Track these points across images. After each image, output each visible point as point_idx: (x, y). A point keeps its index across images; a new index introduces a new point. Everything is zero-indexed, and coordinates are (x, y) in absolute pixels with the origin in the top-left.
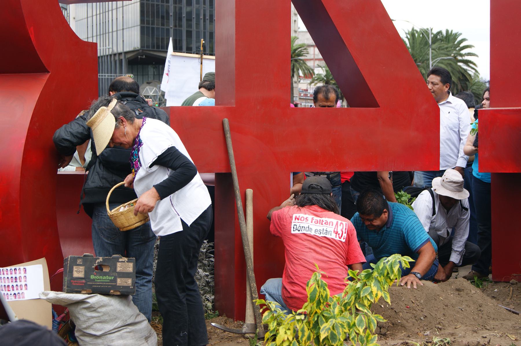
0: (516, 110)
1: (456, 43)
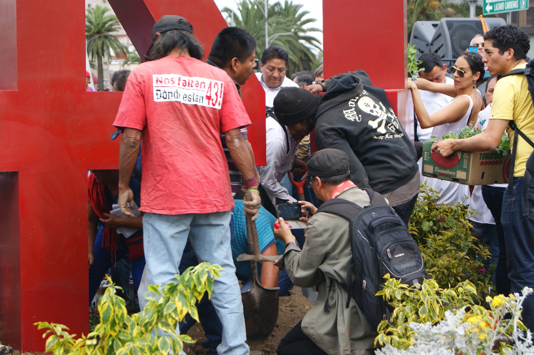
1: (297, 16)
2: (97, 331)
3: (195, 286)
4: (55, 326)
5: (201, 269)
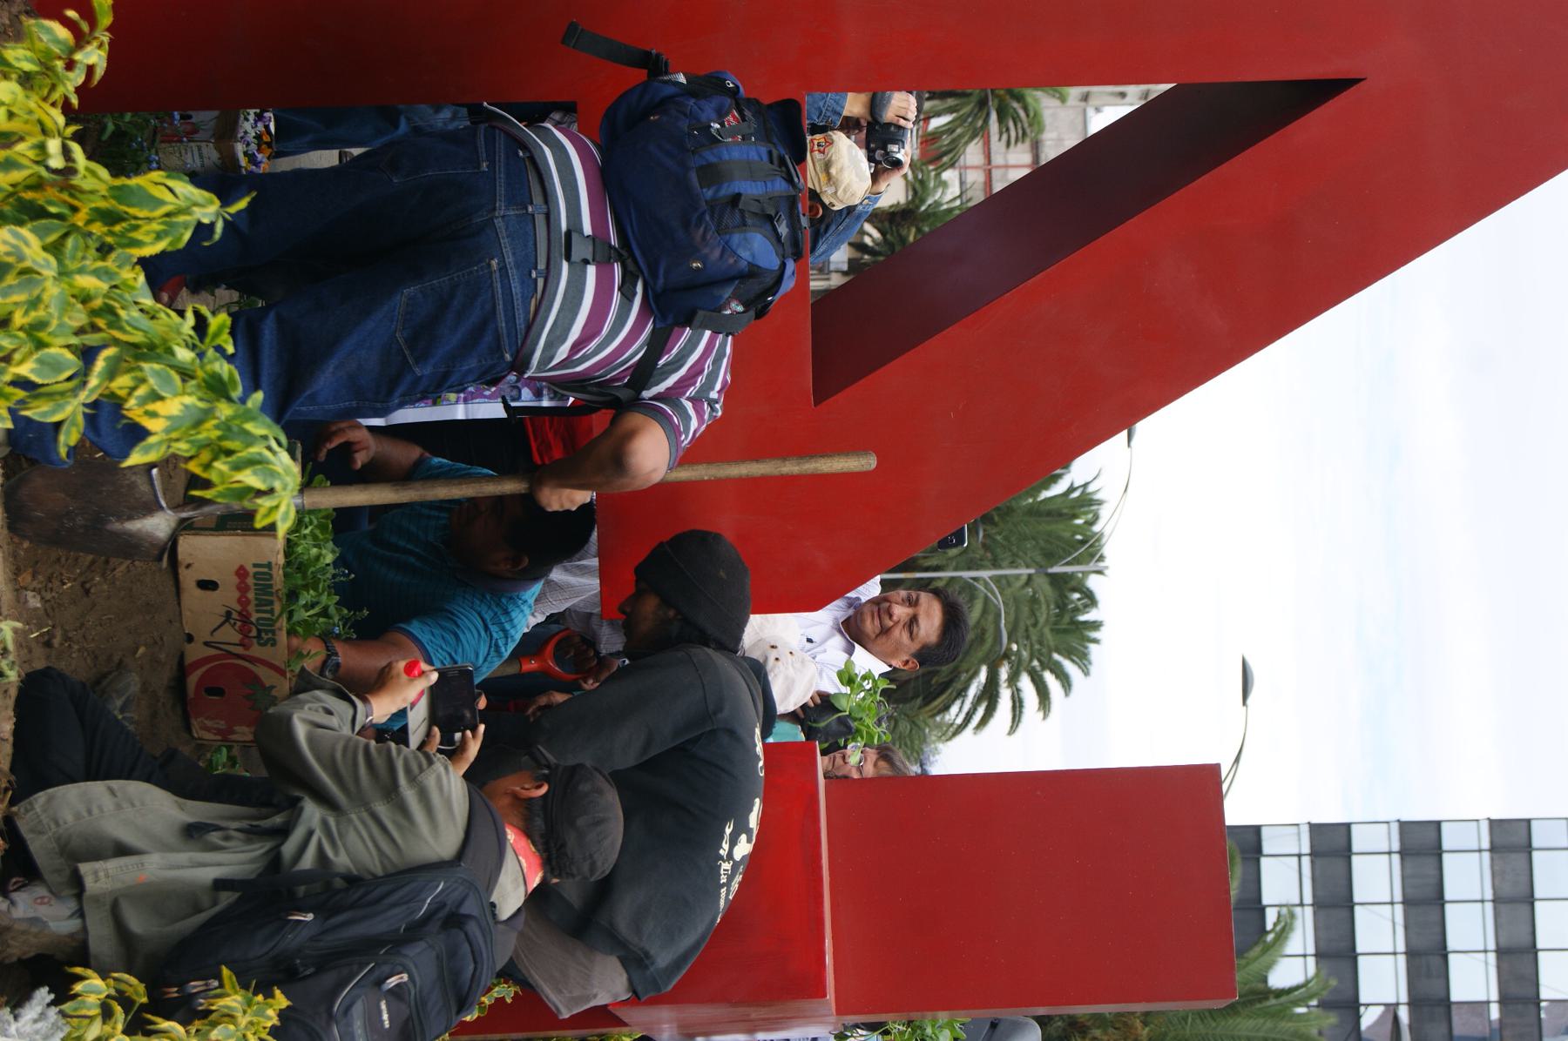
0: (820, 868)
1: (1056, 656)
2: (87, 169)
3: (229, 453)
4: (100, 46)
5: (279, 469)
